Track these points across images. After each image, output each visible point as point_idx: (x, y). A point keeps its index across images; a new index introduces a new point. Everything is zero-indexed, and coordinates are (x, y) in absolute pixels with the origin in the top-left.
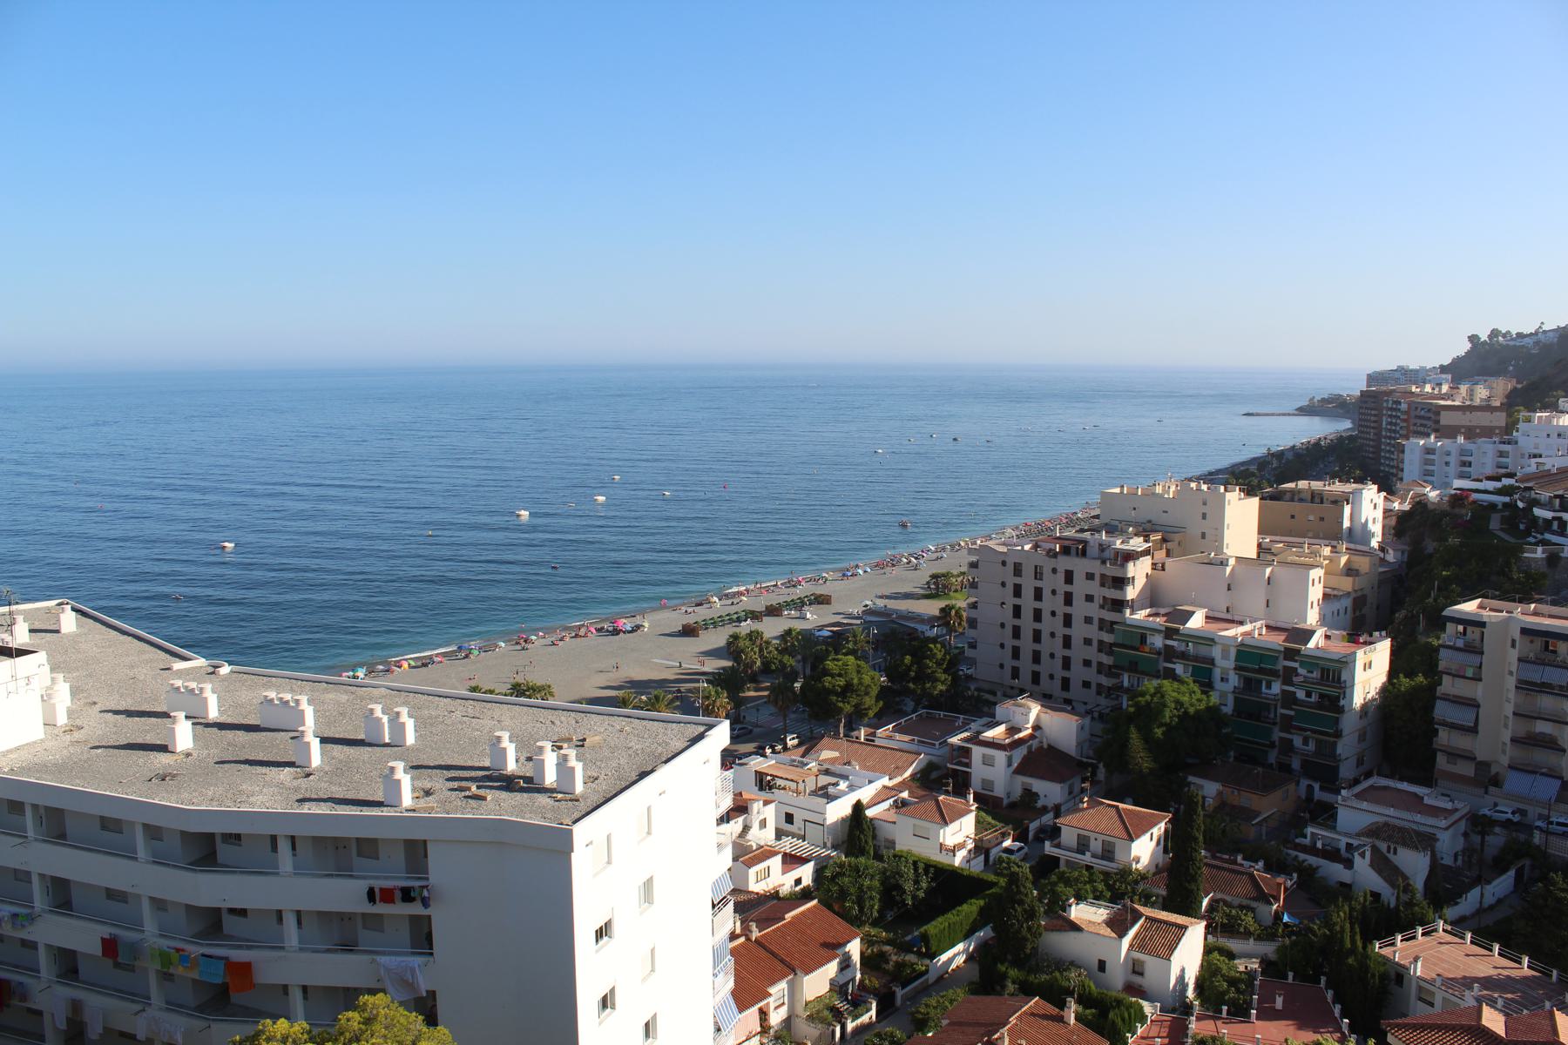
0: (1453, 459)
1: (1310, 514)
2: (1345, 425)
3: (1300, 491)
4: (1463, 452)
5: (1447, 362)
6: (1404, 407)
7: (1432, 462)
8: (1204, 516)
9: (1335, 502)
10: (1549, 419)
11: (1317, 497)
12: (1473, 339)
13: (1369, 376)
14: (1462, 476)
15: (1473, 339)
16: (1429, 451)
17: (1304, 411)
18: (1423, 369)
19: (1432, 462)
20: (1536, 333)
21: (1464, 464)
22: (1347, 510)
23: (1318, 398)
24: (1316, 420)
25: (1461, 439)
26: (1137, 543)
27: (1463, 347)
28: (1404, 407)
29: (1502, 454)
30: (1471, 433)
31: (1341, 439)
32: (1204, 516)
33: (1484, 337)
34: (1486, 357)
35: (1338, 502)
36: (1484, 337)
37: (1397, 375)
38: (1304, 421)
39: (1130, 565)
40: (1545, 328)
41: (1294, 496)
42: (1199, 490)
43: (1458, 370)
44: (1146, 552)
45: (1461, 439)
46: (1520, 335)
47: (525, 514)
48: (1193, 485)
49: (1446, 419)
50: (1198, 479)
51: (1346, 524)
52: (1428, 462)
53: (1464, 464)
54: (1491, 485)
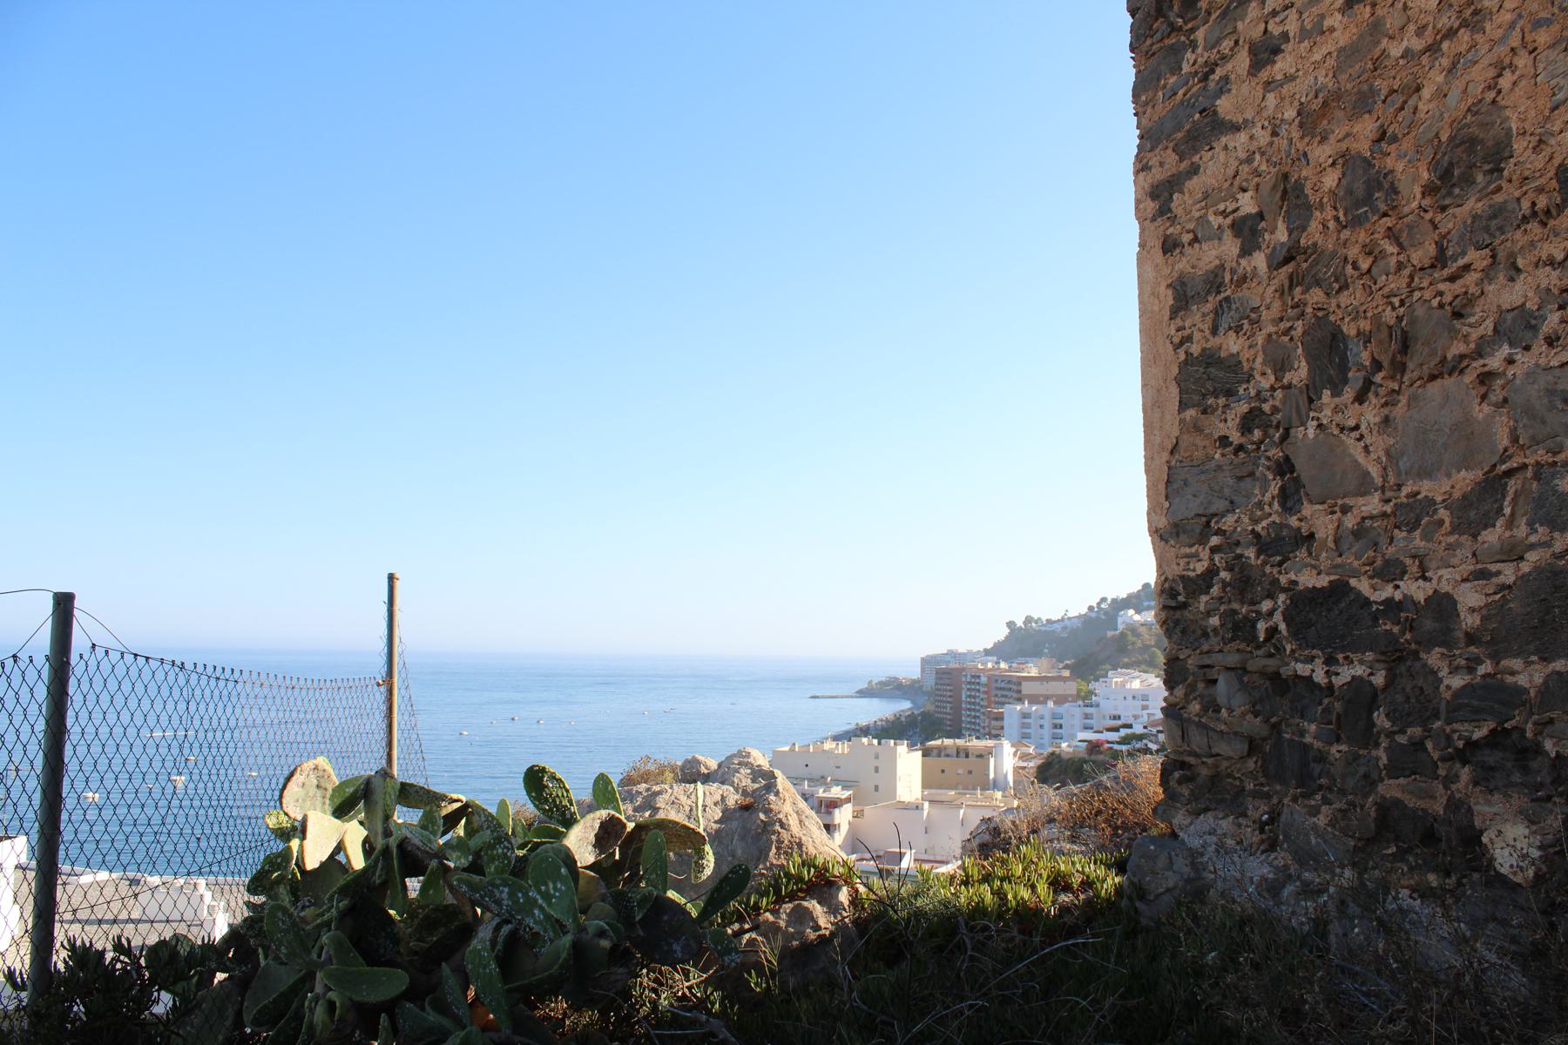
0: (1047, 723)
1: (959, 767)
2: (905, 705)
3: (946, 748)
4: (1054, 716)
5: (989, 646)
6: (984, 680)
7: (1027, 726)
8: (877, 770)
9: (980, 756)
10: (1123, 684)
11: (963, 753)
12: (1010, 624)
13: (923, 660)
14: (1086, 728)
15: (1010, 624)
16: (1025, 715)
17: (862, 694)
18: (970, 652)
19: (1027, 726)
20: (1062, 620)
21: (1055, 726)
22: (992, 761)
23: (875, 681)
24: (875, 702)
25: (1051, 704)
26: (836, 792)
27: (1002, 633)
28: (984, 680)
29: (1087, 716)
30: (1060, 700)
31: (897, 718)
32: (877, 770)
33: (1020, 623)
34: (1025, 640)
35: (983, 756)
36: (1020, 623)
37: (948, 658)
38: (864, 702)
39: (837, 811)
40: (1070, 615)
41: (940, 751)
42: (870, 744)
43: (998, 651)
44: (848, 800)
45: (1051, 704)
46: (1049, 622)
47: (78, 1008)
48: (865, 740)
49: (1027, 688)
50: (836, 738)
51: (992, 776)
52: (1025, 726)
53: (1055, 726)
54: (1114, 736)
